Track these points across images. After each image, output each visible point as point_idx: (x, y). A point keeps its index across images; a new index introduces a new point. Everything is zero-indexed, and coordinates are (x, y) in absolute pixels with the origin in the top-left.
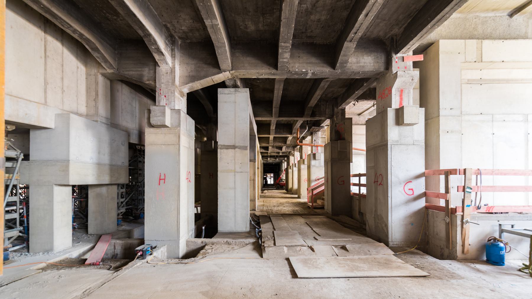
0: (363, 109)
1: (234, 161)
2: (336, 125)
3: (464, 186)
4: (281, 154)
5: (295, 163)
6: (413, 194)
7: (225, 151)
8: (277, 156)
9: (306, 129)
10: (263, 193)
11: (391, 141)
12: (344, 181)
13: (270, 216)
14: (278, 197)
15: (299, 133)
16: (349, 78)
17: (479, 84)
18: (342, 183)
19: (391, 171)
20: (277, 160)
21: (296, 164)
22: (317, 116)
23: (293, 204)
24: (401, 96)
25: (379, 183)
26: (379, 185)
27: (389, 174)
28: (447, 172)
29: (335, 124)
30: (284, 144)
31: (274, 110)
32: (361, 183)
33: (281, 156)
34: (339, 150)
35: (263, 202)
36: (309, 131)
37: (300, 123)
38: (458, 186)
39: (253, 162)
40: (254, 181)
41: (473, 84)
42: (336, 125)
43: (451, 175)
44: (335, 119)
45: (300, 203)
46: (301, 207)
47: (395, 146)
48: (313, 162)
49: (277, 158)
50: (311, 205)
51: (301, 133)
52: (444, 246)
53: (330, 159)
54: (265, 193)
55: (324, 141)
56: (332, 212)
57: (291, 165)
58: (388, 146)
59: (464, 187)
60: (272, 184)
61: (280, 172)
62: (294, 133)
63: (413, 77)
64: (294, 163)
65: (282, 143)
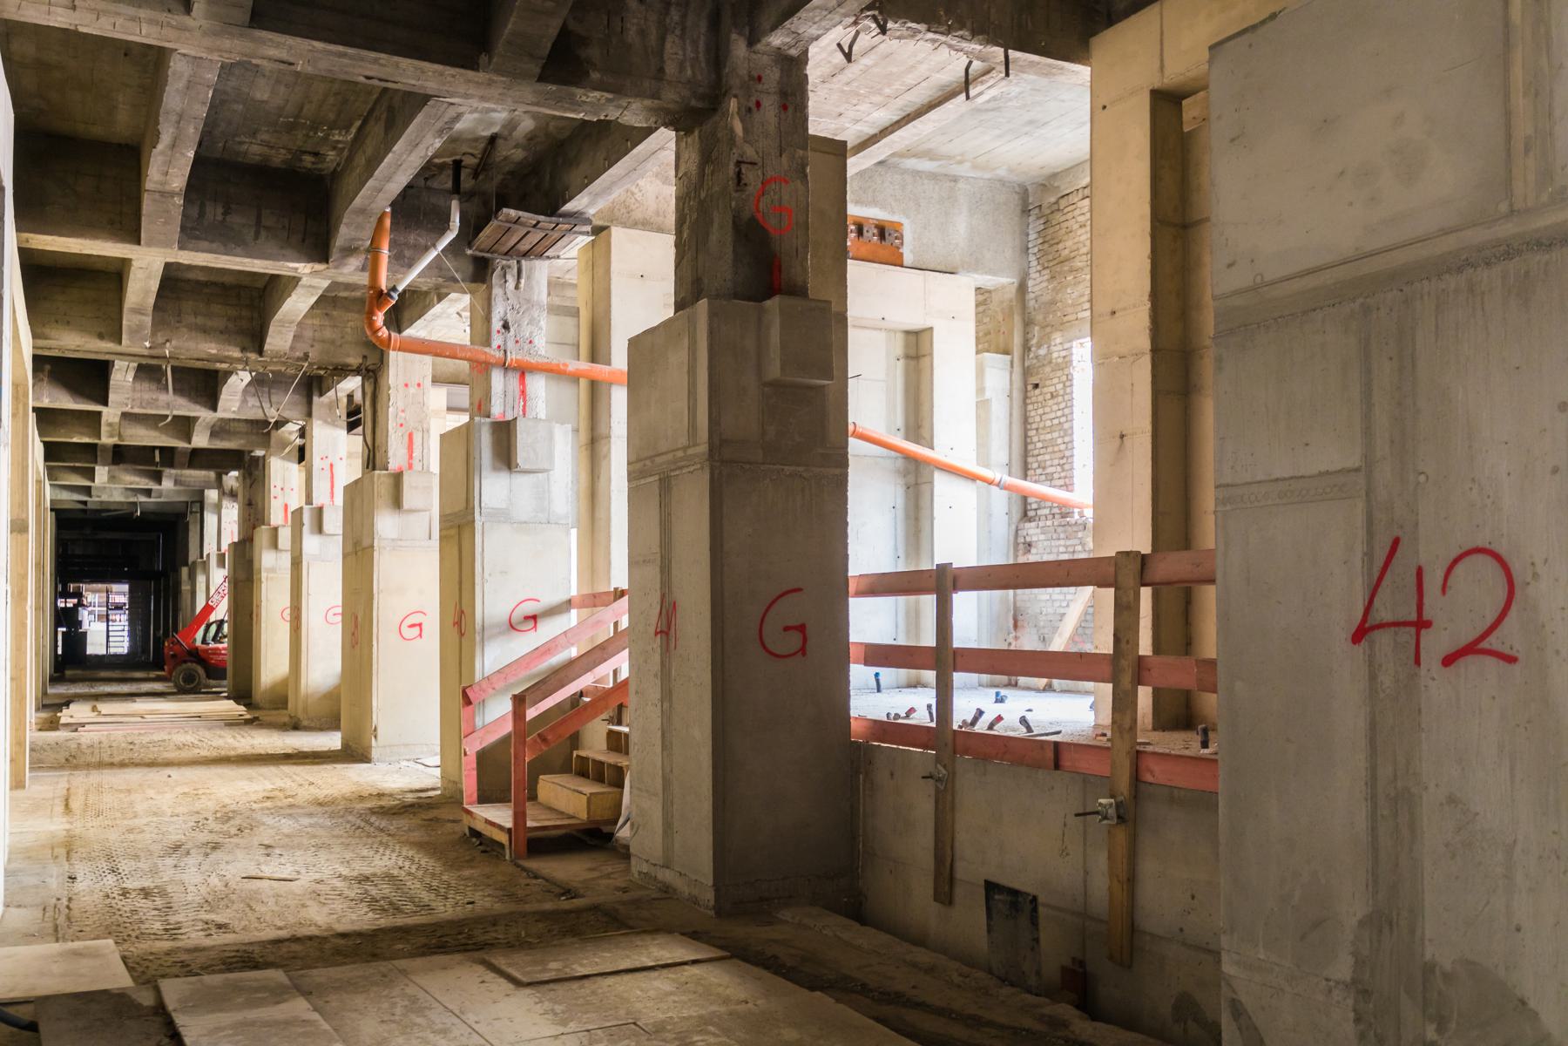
2: (739, 174)
4: (200, 440)
5: (317, 502)
8: (169, 456)
9: (443, 227)
10: (53, 725)
12: (801, 628)
13: (173, 991)
14: (185, 755)
15: (385, 252)
21: (320, 510)
22: (595, 76)
23: (332, 815)
25: (1436, 643)
29: (732, 168)
30: (243, 350)
33: (198, 458)
34: (774, 371)
35: (60, 808)
36: (470, 245)
37: (422, 147)
42: (739, 174)
44: (738, 127)
45: (384, 802)
46: (421, 846)
48: (494, 489)
49: (168, 471)
50: (509, 824)
51: (403, 260)
53: (703, 448)
54: (75, 727)
55: (570, 339)
56: (717, 886)
57: (276, 516)
60: (116, 656)
61: (185, 571)
62: (350, 251)
64: (309, 501)
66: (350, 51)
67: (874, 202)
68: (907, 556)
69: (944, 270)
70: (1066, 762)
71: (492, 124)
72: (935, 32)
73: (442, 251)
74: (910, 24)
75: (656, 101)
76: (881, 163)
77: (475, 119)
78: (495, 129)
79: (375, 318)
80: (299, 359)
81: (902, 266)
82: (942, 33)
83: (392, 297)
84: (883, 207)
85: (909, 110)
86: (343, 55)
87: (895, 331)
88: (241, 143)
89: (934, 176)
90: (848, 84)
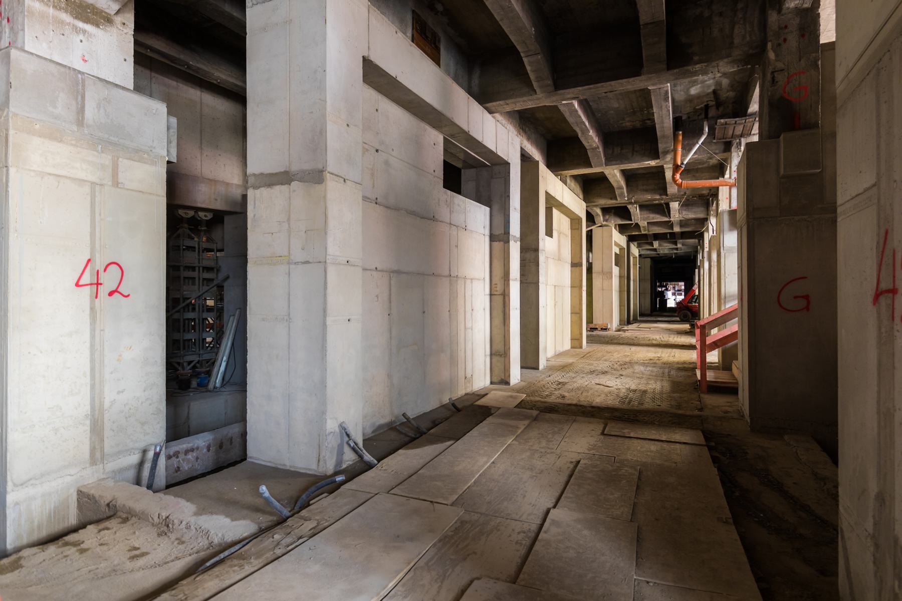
1: (286, 226)
7: (264, 192)
9: (701, 133)
12: (807, 297)
18: (802, 303)
20: (679, 246)
22: (696, 58)
30: (661, 195)
31: (530, 63)
39: (502, 243)
40: (504, 298)
42: (773, 79)
51: (687, 149)
65: (655, 193)
66: (591, 86)
71: (709, 86)
73: (701, 144)
75: (730, 58)
77: (700, 87)
78: (713, 88)
79: (675, 176)
80: (683, 195)
83: (682, 167)
86: (590, 89)
88: (622, 123)
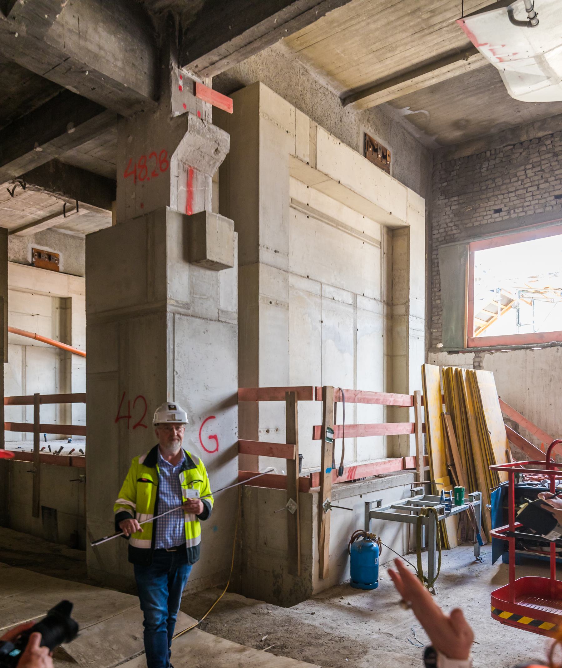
0: (23, 217)
3: (322, 426)
6: (217, 449)
11: (173, 302)
16: (46, 76)
17: (305, 214)
19: (172, 386)
24: (189, 185)
25: (133, 422)
26: (135, 427)
27: (169, 394)
28: (293, 393)
32: (42, 421)
38: (314, 427)
41: (298, 210)
43: (298, 401)
47: (183, 317)
52: (282, 569)
58: (168, 314)
59: (323, 427)
63: (218, 144)
67: (46, 245)
68: (61, 387)
69: (77, 274)
70: (74, 463)
72: (48, 191)
74: (37, 186)
76: (49, 229)
81: (58, 271)
82: (51, 192)
84: (50, 247)
85: (53, 213)
87: (56, 297)
89: (73, 237)
90: (24, 199)
